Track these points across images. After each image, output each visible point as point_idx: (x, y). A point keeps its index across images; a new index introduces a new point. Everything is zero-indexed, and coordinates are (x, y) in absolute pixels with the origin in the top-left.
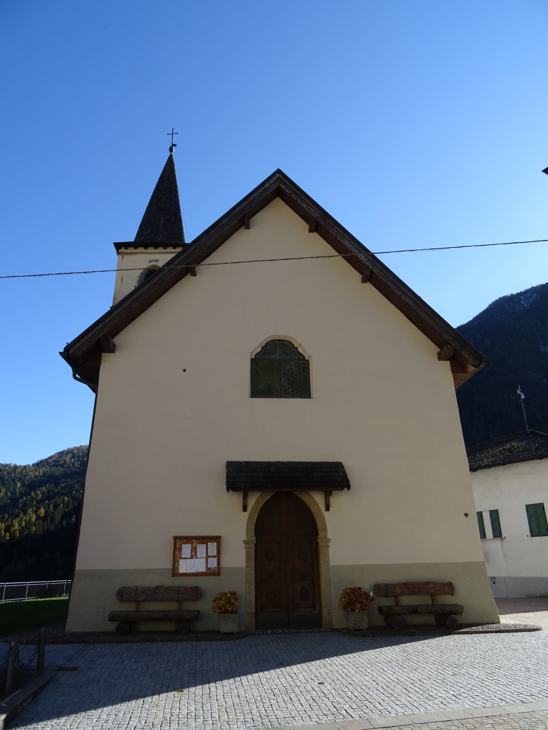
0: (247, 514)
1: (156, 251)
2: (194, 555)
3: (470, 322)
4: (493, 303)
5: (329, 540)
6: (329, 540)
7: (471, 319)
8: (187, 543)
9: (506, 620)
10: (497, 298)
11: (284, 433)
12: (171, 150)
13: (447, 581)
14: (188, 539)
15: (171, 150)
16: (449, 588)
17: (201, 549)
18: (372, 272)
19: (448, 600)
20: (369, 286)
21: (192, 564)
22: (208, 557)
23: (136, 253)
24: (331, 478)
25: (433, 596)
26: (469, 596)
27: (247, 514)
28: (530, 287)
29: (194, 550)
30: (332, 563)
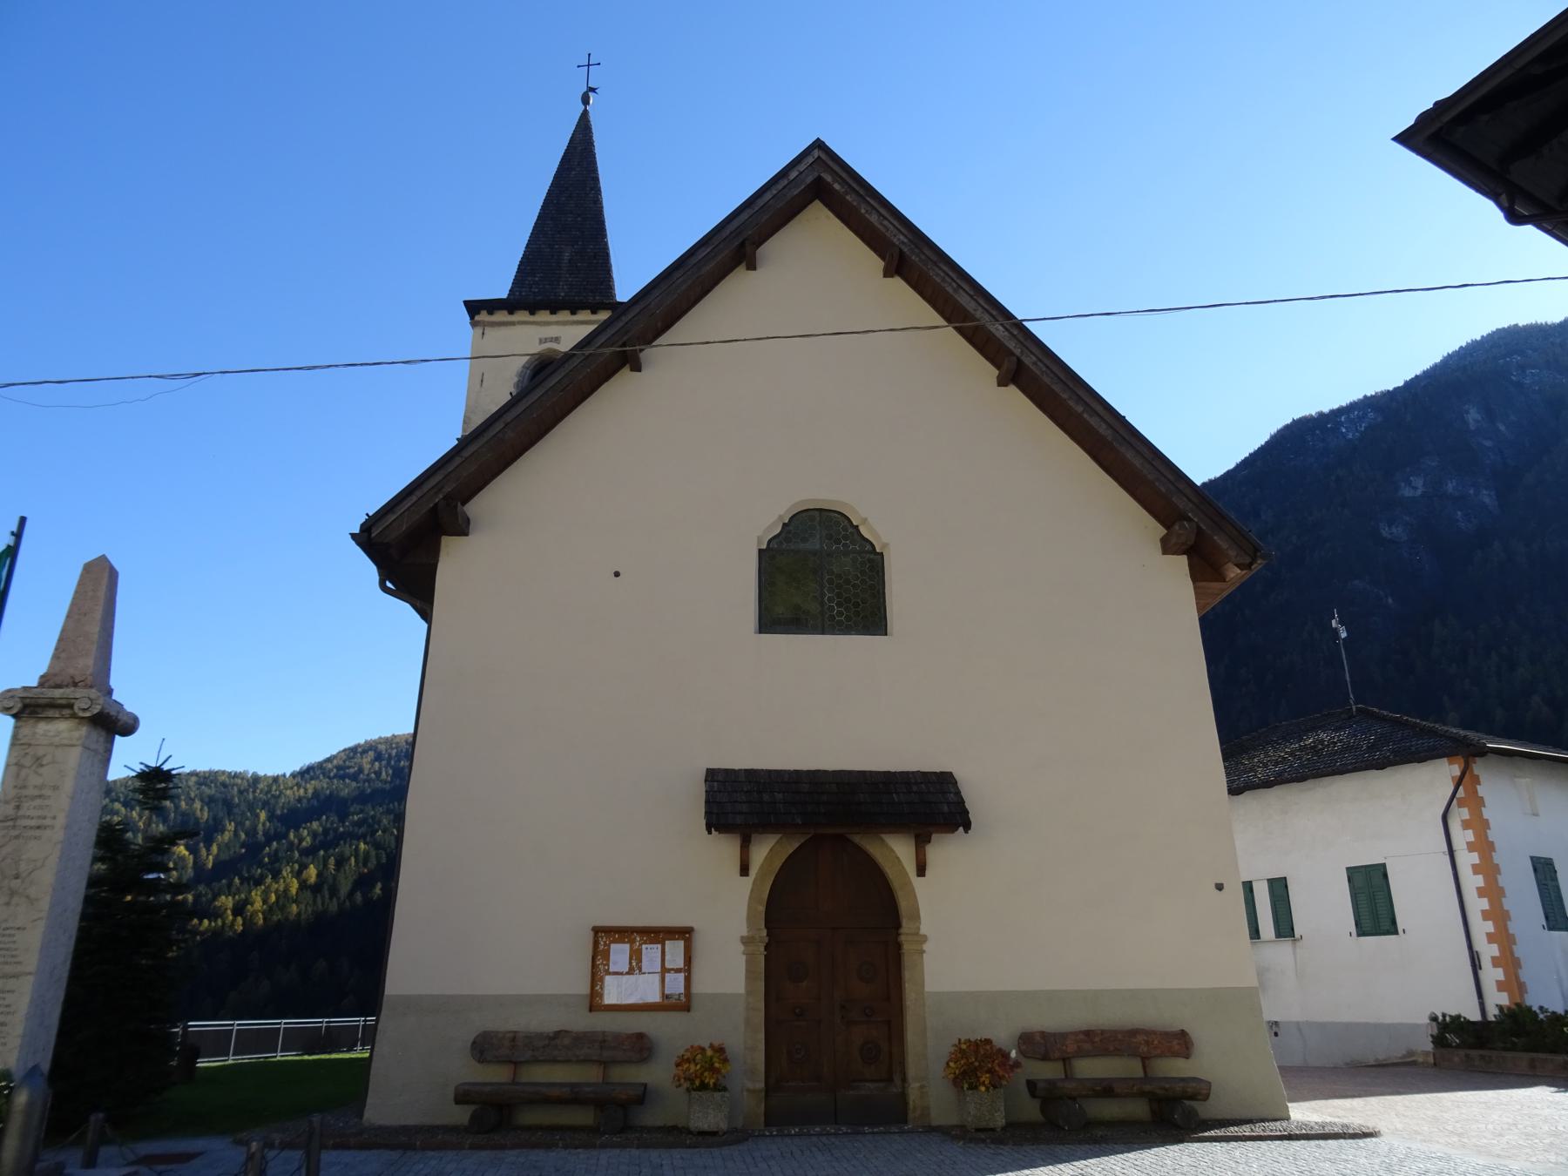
0: (748, 882)
1: (554, 318)
2: (635, 967)
5: (924, 939)
6: (924, 939)
7: (1232, 466)
9: (1303, 1113)
10: (1289, 421)
11: (829, 709)
12: (585, 100)
13: (1177, 1027)
15: (585, 100)
16: (1180, 1043)
17: (651, 953)
22: (664, 970)
23: (513, 324)
24: (931, 805)
25: (1145, 1060)
26: (1220, 1061)
27: (748, 882)
29: (636, 956)
30: (930, 986)
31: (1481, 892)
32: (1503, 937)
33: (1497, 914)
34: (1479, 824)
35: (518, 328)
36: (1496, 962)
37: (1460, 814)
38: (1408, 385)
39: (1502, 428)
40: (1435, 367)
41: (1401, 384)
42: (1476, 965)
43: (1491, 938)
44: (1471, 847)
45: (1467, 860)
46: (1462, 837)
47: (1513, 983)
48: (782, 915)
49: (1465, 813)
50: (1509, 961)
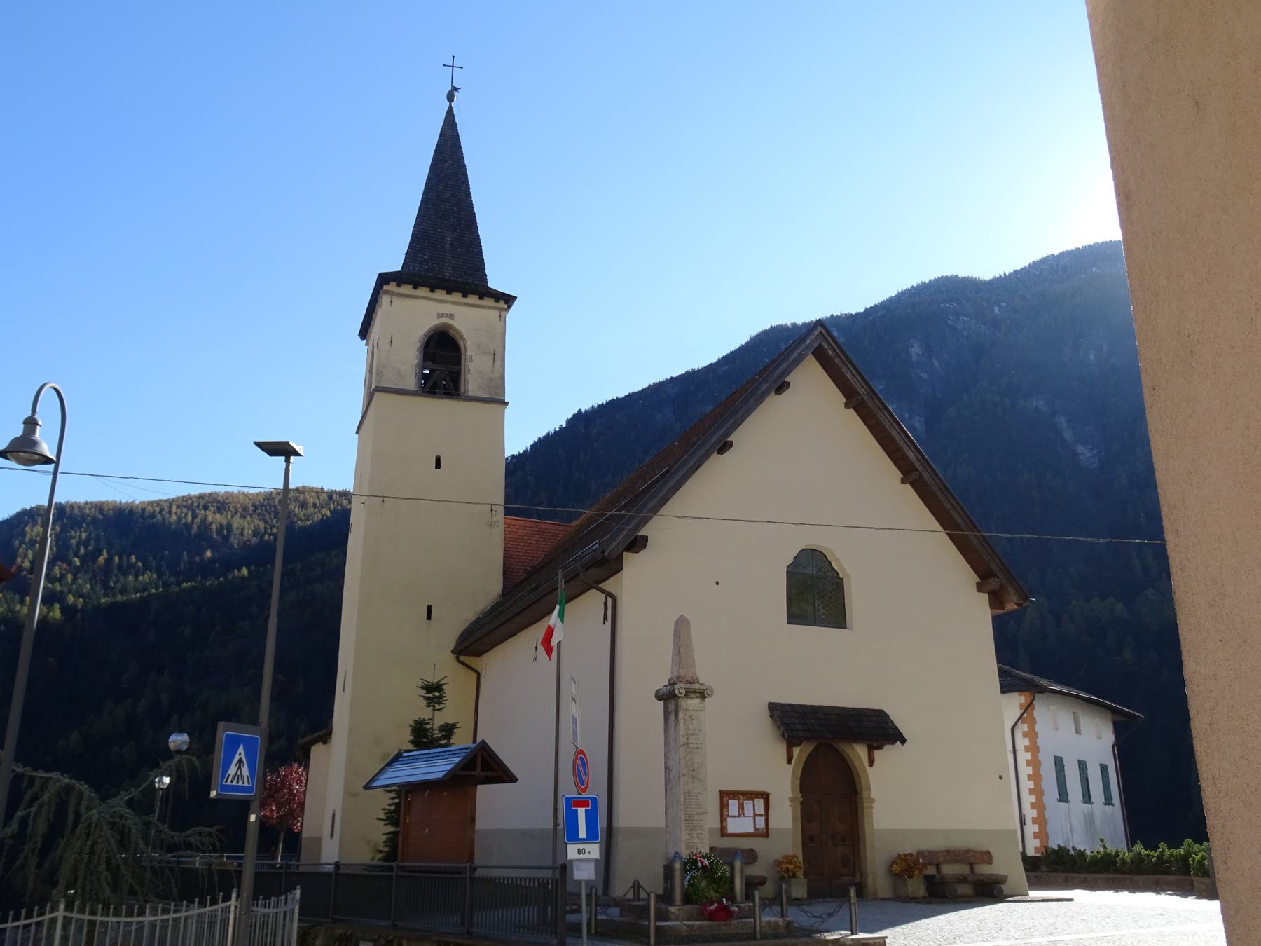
0: (791, 767)
1: (449, 298)
2: (741, 813)
3: (711, 365)
4: (758, 335)
5: (873, 801)
6: (873, 801)
7: (714, 360)
8: (733, 799)
9: (1033, 894)
10: (768, 327)
11: (828, 671)
12: (450, 98)
13: (985, 849)
14: (734, 795)
15: (450, 98)
16: (987, 857)
17: (748, 805)
18: (921, 476)
19: (984, 870)
20: (908, 488)
21: (740, 824)
22: (755, 815)
23: (416, 297)
24: (878, 730)
25: (971, 865)
26: (1009, 866)
27: (791, 767)
28: (829, 315)
29: (741, 806)
30: (875, 827)
31: (1030, 777)
32: (1039, 806)
33: (1037, 792)
34: (1032, 735)
35: (419, 302)
36: (1034, 821)
37: (1022, 727)
38: (868, 311)
39: (936, 364)
40: (891, 300)
41: (862, 310)
42: (1022, 823)
43: (1033, 806)
44: (1027, 749)
45: (1024, 756)
46: (1022, 742)
47: (1042, 835)
48: (808, 783)
49: (1025, 727)
50: (1041, 820)
